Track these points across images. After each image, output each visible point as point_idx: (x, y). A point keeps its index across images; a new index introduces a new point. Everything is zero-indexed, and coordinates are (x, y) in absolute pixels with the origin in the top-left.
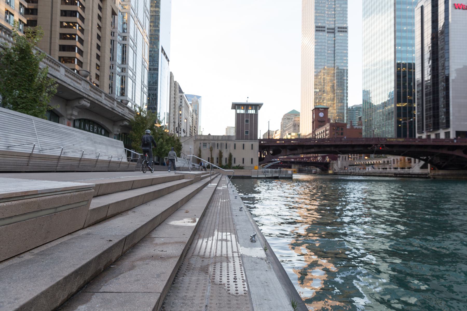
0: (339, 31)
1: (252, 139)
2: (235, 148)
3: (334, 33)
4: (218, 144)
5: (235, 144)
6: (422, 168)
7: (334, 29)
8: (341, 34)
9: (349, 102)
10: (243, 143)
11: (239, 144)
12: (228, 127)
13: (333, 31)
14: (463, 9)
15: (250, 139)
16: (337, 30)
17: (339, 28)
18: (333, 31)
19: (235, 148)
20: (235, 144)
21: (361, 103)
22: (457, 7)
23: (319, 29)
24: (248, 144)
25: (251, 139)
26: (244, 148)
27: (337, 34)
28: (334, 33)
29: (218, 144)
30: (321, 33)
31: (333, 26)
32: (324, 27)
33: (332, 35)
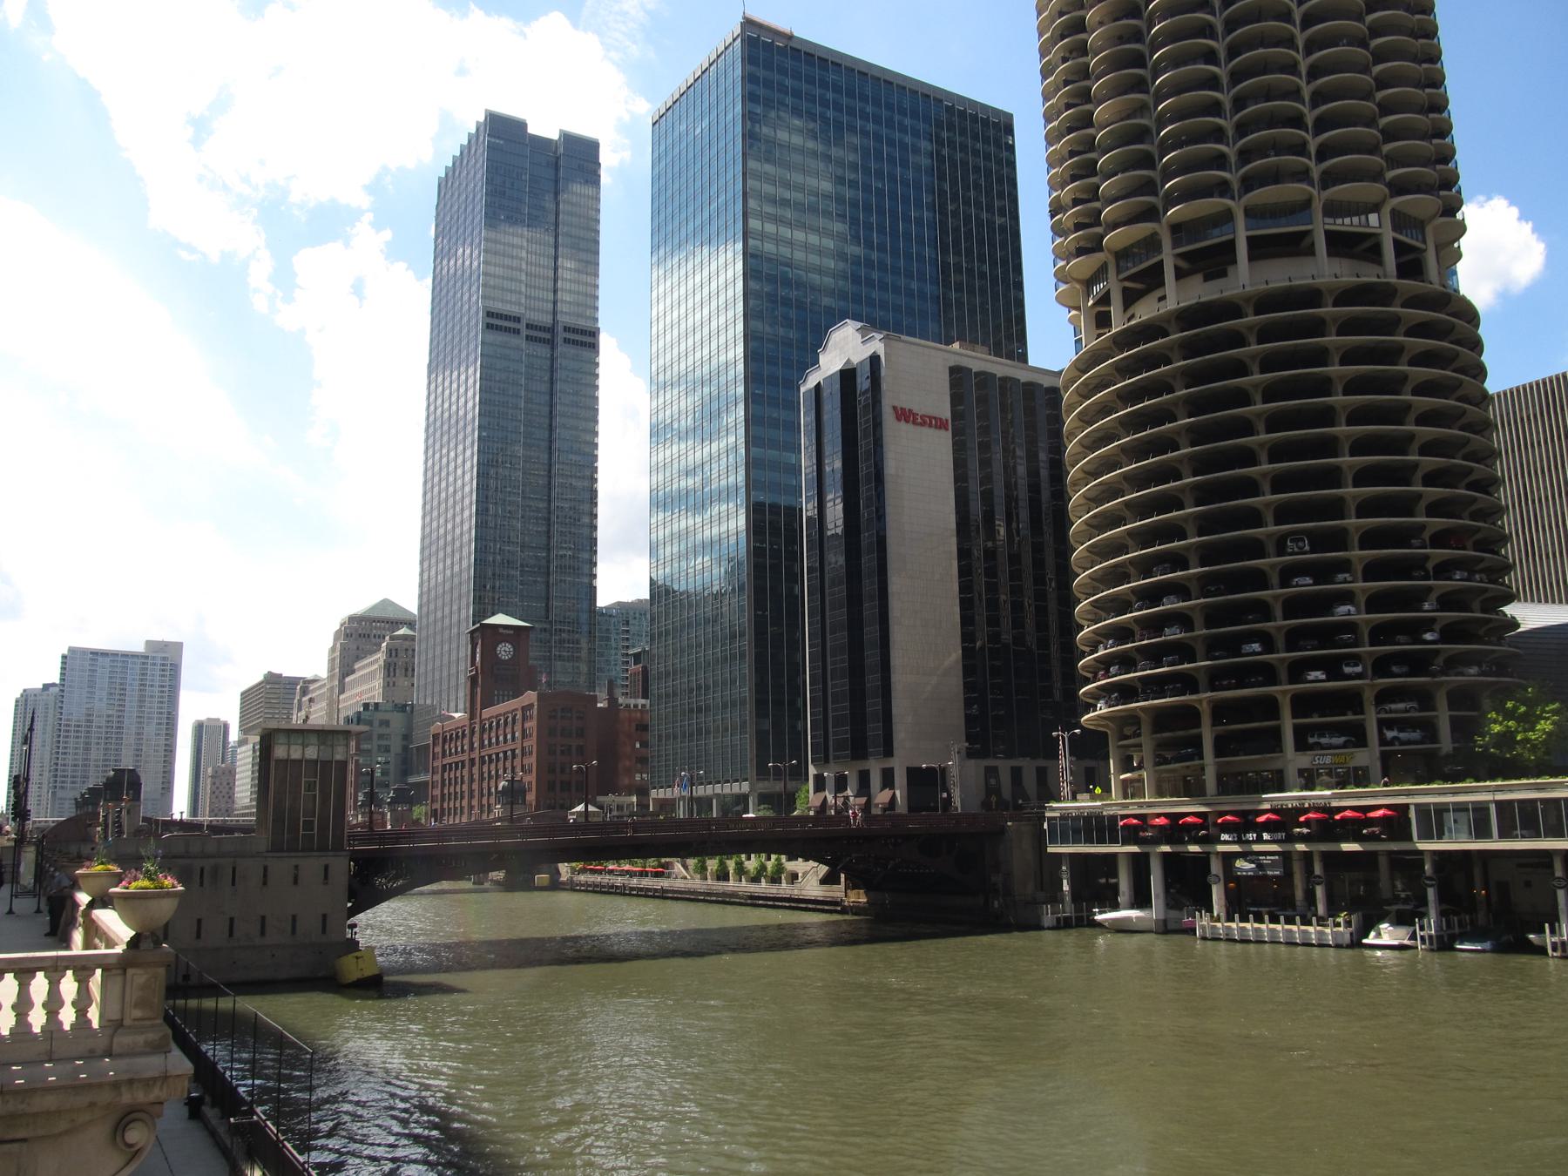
0: (566, 341)
1: (327, 849)
2: (265, 883)
3: (551, 343)
4: (202, 870)
5: (265, 869)
6: (823, 882)
7: (551, 330)
8: (571, 350)
9: (600, 583)
10: (294, 862)
11: (281, 867)
12: (71, 650)
13: (547, 336)
14: (914, 423)
15: (319, 850)
16: (561, 335)
17: (566, 329)
18: (547, 336)
19: (265, 883)
20: (265, 869)
21: (645, 594)
23: (497, 322)
24: (311, 865)
25: (323, 848)
26: (296, 882)
27: (561, 349)
28: (551, 343)
29: (202, 870)
30: (500, 338)
31: (547, 320)
32: (517, 320)
33: (543, 351)
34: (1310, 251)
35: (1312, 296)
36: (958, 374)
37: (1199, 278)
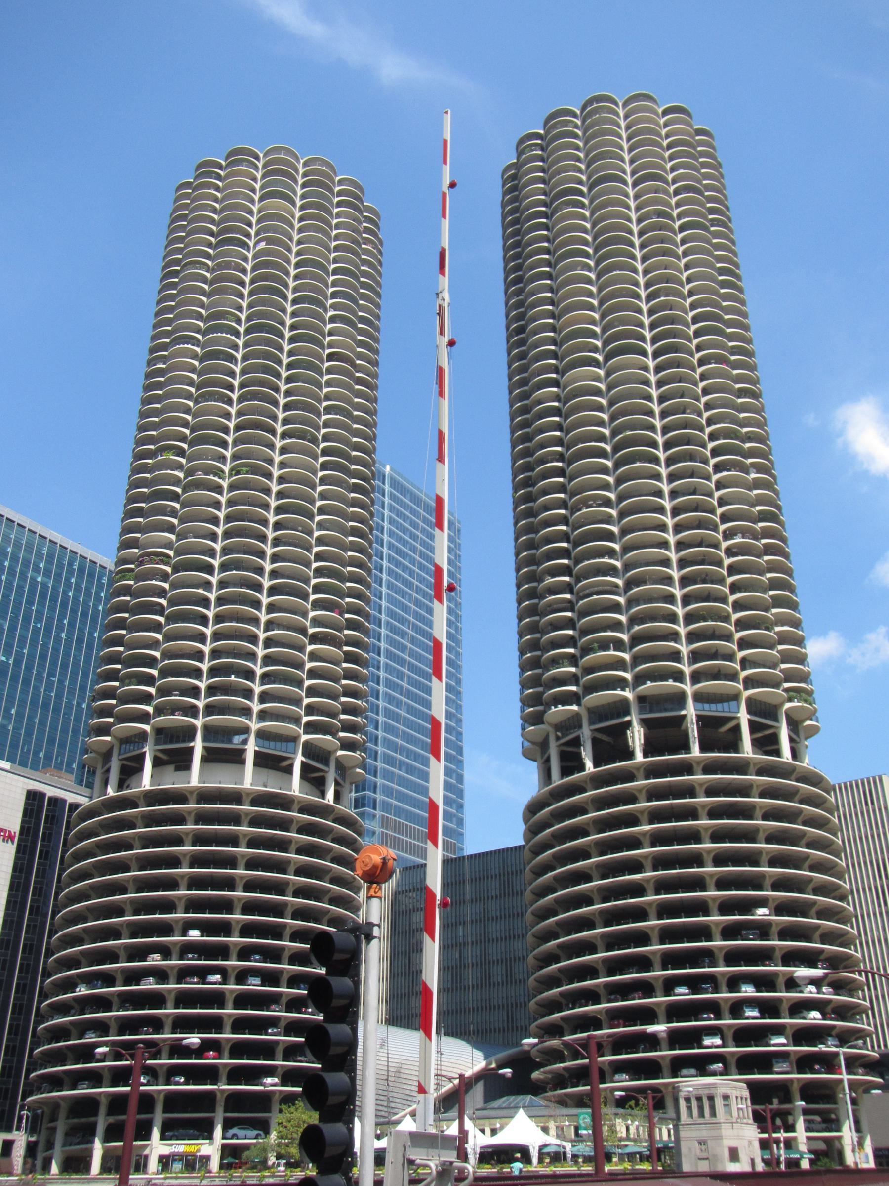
22: (11, 837)
34: (243, 762)
35: (236, 797)
36: (34, 799)
37: (171, 768)
